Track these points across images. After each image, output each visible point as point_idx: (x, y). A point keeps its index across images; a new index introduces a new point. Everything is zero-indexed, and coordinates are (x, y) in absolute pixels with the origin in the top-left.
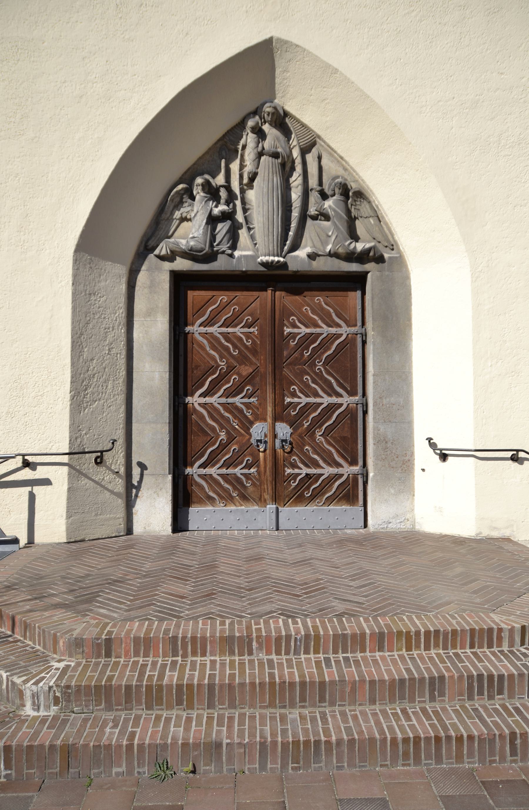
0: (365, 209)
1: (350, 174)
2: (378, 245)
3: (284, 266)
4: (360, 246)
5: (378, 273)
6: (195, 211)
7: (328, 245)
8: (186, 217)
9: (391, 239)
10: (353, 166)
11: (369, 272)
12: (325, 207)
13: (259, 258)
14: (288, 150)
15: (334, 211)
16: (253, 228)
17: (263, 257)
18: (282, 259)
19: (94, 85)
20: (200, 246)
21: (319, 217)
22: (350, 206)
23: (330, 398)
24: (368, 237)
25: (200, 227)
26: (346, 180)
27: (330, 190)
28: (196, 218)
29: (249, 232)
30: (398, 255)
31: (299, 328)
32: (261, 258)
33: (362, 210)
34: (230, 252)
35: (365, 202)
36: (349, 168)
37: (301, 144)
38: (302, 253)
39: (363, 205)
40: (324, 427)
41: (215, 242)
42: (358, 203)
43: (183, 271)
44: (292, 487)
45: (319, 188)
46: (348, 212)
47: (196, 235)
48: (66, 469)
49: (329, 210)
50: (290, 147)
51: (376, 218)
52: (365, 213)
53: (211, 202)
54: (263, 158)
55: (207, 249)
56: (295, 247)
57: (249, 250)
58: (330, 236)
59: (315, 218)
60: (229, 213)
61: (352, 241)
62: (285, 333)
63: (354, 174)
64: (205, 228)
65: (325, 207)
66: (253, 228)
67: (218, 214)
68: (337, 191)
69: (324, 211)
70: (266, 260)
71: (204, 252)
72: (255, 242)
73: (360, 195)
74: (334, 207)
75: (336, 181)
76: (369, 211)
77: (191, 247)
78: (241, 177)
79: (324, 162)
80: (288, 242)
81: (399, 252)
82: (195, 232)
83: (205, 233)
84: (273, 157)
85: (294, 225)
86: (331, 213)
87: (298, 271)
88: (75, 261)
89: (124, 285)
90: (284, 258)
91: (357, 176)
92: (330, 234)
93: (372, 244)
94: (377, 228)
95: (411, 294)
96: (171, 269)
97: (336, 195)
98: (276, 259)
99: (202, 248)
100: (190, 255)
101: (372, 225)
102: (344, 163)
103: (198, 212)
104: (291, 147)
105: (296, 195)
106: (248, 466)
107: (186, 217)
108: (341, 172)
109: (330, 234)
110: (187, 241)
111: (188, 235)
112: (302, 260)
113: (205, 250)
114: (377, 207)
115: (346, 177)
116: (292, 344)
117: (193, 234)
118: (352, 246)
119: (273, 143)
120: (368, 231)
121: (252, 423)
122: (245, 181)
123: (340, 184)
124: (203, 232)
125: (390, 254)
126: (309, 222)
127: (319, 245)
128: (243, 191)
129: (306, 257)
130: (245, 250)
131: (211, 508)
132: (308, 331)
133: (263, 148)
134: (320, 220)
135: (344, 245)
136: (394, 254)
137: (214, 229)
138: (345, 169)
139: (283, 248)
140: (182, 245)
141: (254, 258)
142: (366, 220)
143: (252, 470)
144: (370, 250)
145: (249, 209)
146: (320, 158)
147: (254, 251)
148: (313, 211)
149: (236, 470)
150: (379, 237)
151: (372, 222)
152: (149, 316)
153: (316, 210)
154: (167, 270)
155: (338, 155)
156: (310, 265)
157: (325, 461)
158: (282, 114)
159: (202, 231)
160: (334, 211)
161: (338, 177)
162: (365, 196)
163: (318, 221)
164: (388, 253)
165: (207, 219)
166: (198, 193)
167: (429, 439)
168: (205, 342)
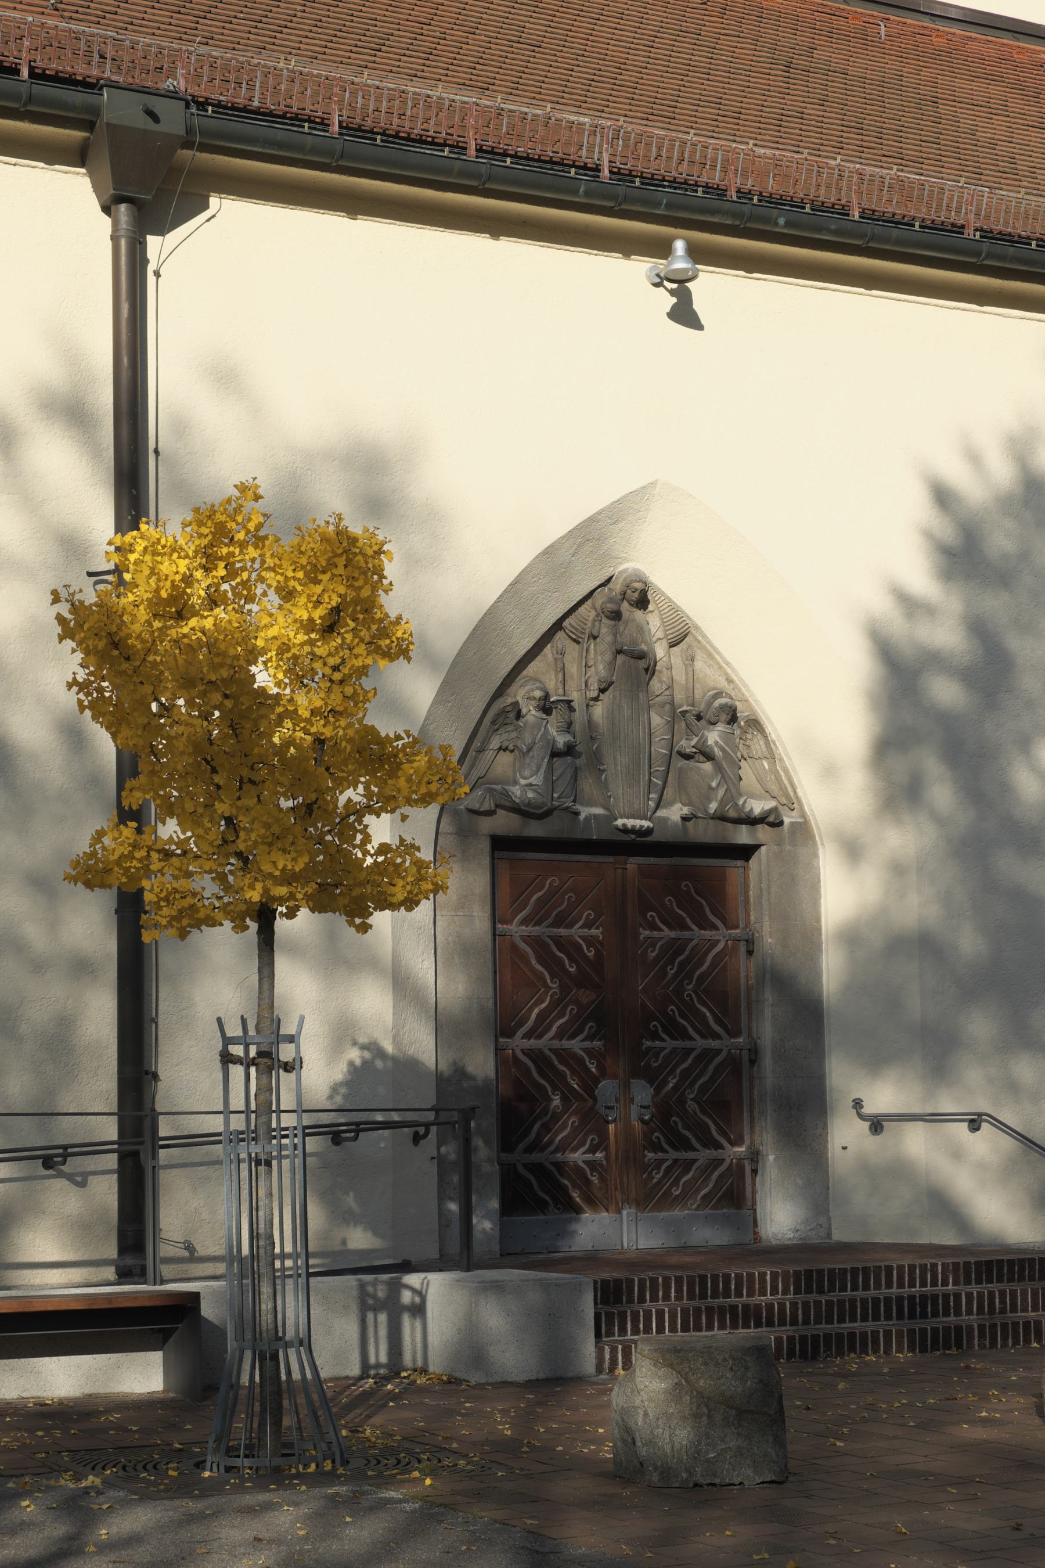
0: (757, 747)
1: (736, 687)
2: (780, 806)
3: (649, 831)
7: (710, 801)
16: (604, 771)
18: (646, 824)
23: (704, 1041)
28: (531, 754)
30: (801, 820)
31: (660, 930)
33: (753, 747)
35: (759, 736)
36: (735, 678)
39: (755, 740)
40: (696, 1087)
42: (749, 736)
44: (655, 1180)
48: (116, 1155)
59: (688, 757)
62: (642, 937)
66: (604, 771)
69: (707, 750)
71: (545, 809)
73: (755, 724)
76: (764, 749)
81: (803, 815)
86: (718, 752)
91: (746, 693)
92: (714, 784)
95: (819, 881)
98: (638, 823)
102: (729, 671)
106: (593, 1150)
108: (722, 683)
109: (714, 784)
116: (652, 955)
121: (597, 1081)
129: (679, 819)
131: (542, 1217)
132: (673, 934)
135: (736, 804)
138: (730, 681)
143: (599, 1155)
149: (576, 1155)
151: (767, 767)
152: (462, 907)
156: (685, 828)
157: (699, 1140)
160: (722, 749)
161: (719, 695)
163: (691, 763)
164: (791, 817)
167: (219, 1020)
168: (528, 950)
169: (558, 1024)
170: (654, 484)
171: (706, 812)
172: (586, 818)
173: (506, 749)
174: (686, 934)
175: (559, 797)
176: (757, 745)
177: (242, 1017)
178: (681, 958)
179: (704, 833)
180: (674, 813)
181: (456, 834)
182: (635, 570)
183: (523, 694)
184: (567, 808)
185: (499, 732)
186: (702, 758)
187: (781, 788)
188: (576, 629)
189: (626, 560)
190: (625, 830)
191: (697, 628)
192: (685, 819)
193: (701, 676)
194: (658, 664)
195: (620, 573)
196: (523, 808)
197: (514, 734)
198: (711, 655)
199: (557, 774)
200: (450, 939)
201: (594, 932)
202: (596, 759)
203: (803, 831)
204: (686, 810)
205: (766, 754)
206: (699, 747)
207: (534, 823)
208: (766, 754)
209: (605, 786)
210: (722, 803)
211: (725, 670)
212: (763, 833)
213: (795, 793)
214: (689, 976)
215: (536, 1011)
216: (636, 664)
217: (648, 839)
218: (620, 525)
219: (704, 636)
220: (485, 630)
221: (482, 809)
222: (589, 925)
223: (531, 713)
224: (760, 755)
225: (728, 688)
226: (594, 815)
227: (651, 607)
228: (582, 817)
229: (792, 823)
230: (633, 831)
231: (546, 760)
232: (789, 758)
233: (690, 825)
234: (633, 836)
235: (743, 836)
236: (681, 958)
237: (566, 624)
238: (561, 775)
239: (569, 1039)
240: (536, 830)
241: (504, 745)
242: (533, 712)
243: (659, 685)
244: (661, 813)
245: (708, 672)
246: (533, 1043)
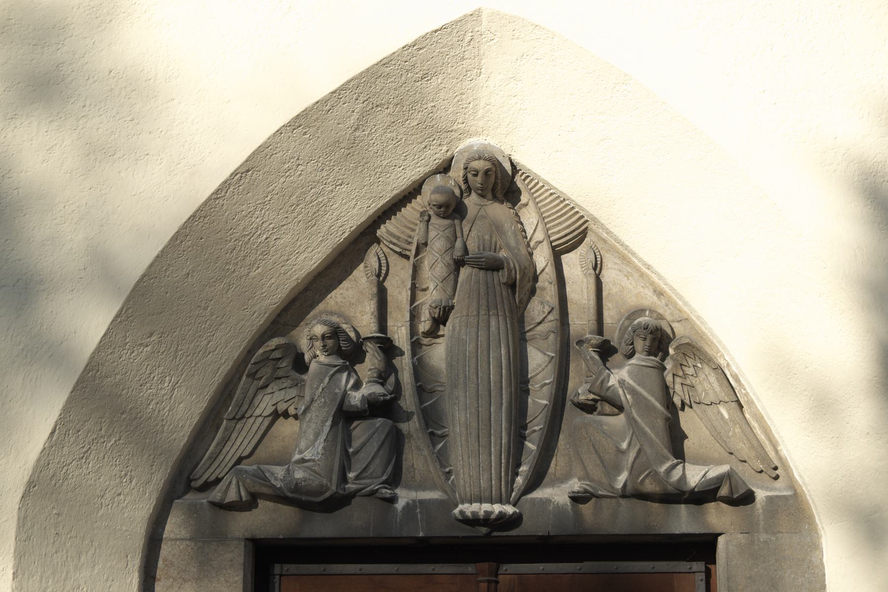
0: (706, 384)
1: (670, 302)
2: (740, 469)
3: (515, 521)
4: (695, 476)
5: (740, 536)
6: (307, 398)
7: (619, 472)
8: (286, 410)
9: (772, 454)
10: (675, 287)
11: (720, 534)
12: (610, 384)
13: (457, 506)
14: (523, 251)
15: (633, 392)
16: (443, 436)
17: (466, 505)
18: (509, 509)
19: (81, 122)
20: (315, 482)
21: (599, 405)
22: (669, 379)
24: (717, 450)
25: (317, 435)
26: (661, 317)
27: (623, 344)
28: (308, 416)
29: (434, 445)
30: (788, 493)
32: (460, 507)
33: (699, 388)
34: (386, 492)
35: (707, 369)
36: (666, 288)
37: (554, 244)
38: (556, 494)
39: (702, 376)
41: (350, 446)
42: (690, 371)
43: (278, 539)
45: (596, 339)
46: (666, 392)
47: (307, 455)
49: (621, 392)
50: (528, 245)
51: (734, 405)
52: (707, 394)
53: (345, 375)
54: (464, 272)
55: (334, 488)
56: (536, 480)
57: (433, 487)
58: (623, 452)
59: (588, 408)
60: (385, 401)
61: (675, 461)
63: (680, 303)
64: (330, 438)
65: (610, 384)
66: (443, 436)
67: (359, 404)
68: (640, 345)
69: (609, 394)
70: (472, 513)
71: (327, 495)
72: (447, 470)
73: (696, 351)
74: (631, 382)
75: (636, 322)
77: (297, 484)
78: (414, 316)
79: (609, 276)
80: (524, 469)
81: (792, 485)
82: (307, 448)
83: (328, 450)
84: (487, 269)
85: (536, 426)
86: (626, 398)
87: (549, 537)
88: (22, 522)
89: (136, 575)
90: (514, 505)
91: (685, 309)
92: (624, 445)
93: (724, 469)
94: (737, 430)
96: (248, 536)
97: (637, 355)
98: (497, 508)
99: (322, 486)
100: (296, 498)
101: (725, 422)
102: (655, 279)
103: (312, 401)
104: (532, 244)
105: (539, 360)
107: (286, 410)
108: (648, 298)
110: (288, 470)
111: (291, 457)
112: (560, 510)
113: (328, 489)
114: (737, 380)
115: (661, 311)
117: (301, 452)
118: (677, 474)
119: (487, 237)
120: (717, 436)
122: (424, 326)
123: (646, 328)
124: (324, 448)
125: (771, 490)
126: (572, 418)
127: (597, 472)
128: (416, 346)
129: (568, 501)
130: (424, 489)
133: (466, 251)
134: (600, 414)
135: (656, 473)
136: (780, 489)
137: (348, 440)
138: (659, 293)
139: (513, 481)
140: (276, 479)
141: (448, 505)
142: (710, 410)
144: (720, 480)
145: (432, 392)
146: (597, 267)
147: (445, 492)
148: (584, 394)
150: (743, 448)
151: (726, 415)
153: (590, 392)
154: (238, 539)
155: (640, 260)
156: (578, 515)
158: (510, 173)
159: (322, 445)
161: (641, 311)
162: (705, 354)
163: (594, 417)
164: (767, 489)
165: (334, 416)
166: (315, 356)
170: (475, 16)
171: (613, 488)
172: (408, 508)
173: (286, 415)
175: (357, 478)
176: (707, 384)
179: (623, 519)
180: (556, 494)
181: (191, 539)
182: (485, 146)
183: (309, 335)
184: (372, 493)
185: (269, 390)
186: (608, 408)
187: (752, 447)
188: (398, 238)
189: (466, 134)
190: (473, 521)
191: (595, 220)
192: (577, 499)
193: (614, 290)
194: (541, 278)
195: (460, 152)
196: (289, 494)
197: (293, 392)
198: (625, 258)
199: (356, 444)
202: (433, 421)
203: (793, 509)
204: (576, 485)
205: (723, 396)
206: (596, 390)
207: (319, 517)
208: (723, 396)
209: (442, 458)
210: (634, 471)
211: (647, 276)
212: (717, 517)
213: (777, 452)
216: (507, 284)
217: (513, 533)
218: (435, 82)
219: (609, 232)
220: (207, 234)
221: (227, 500)
223: (319, 359)
224: (712, 398)
225: (660, 305)
226: (422, 502)
227: (524, 198)
228: (400, 505)
229: (770, 500)
230: (486, 521)
231: (329, 423)
232: (759, 400)
233: (587, 509)
234: (484, 530)
235: (682, 521)
237: (381, 232)
238: (363, 445)
240: (324, 527)
241: (281, 407)
242: (322, 358)
243: (540, 307)
244: (538, 494)
245: (627, 283)
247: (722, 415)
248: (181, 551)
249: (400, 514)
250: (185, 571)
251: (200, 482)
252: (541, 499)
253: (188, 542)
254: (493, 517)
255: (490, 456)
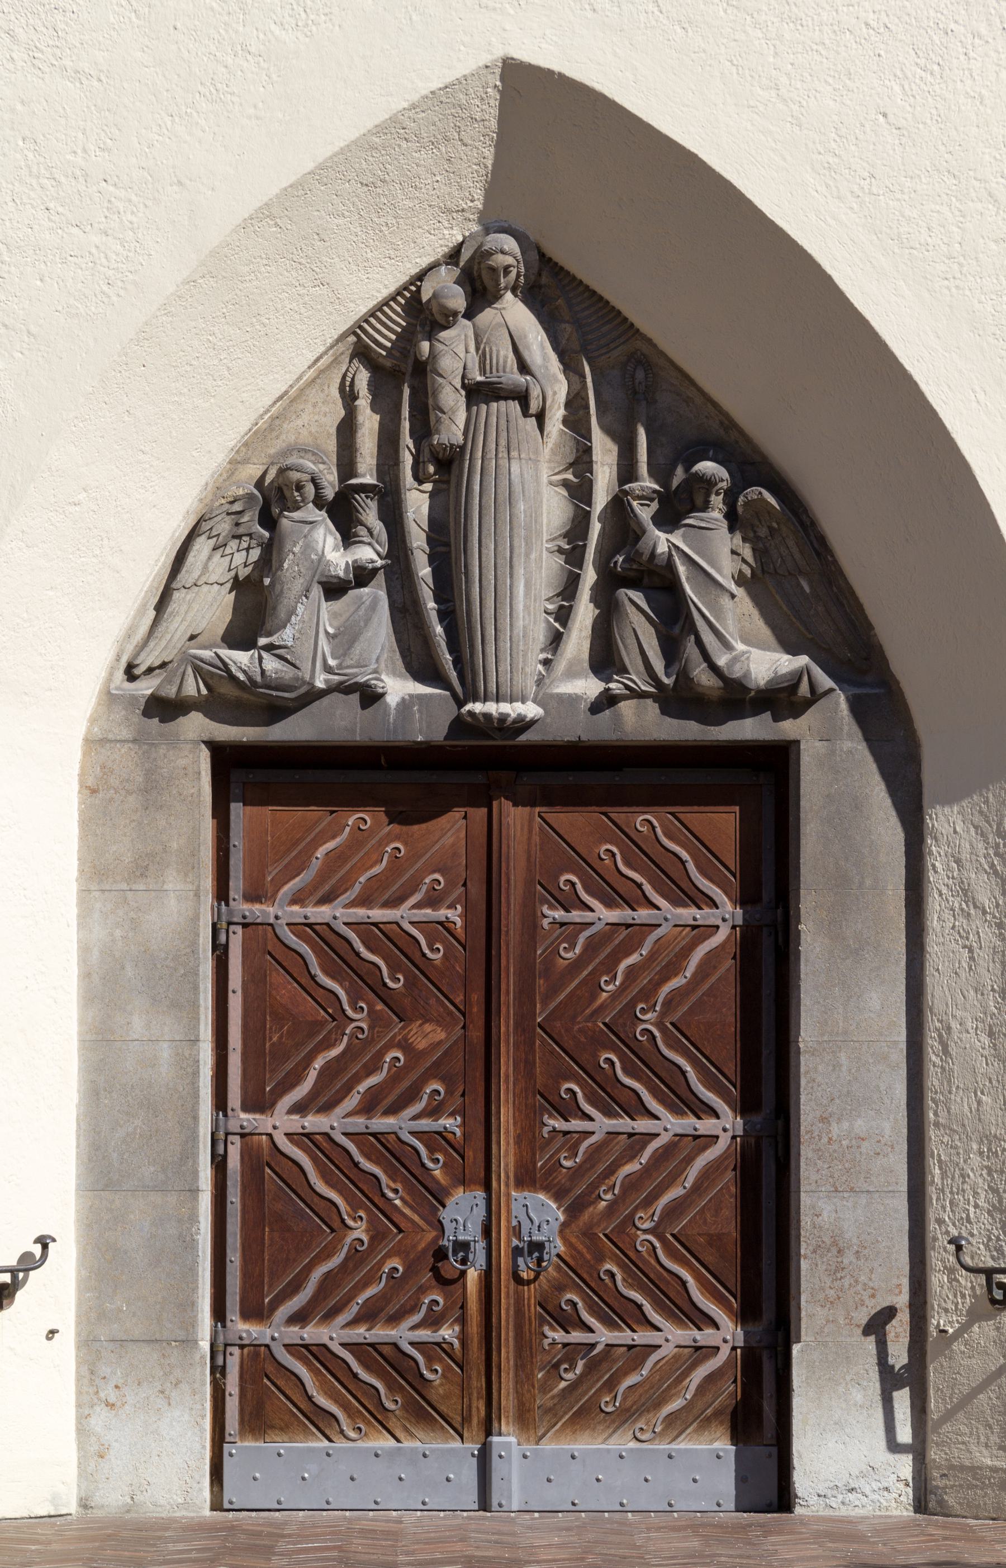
5: (818, 744)
151: (807, 589)
157: (660, 1307)
169: (362, 1088)
174: (643, 915)
177: (718, 1329)
178: (633, 959)
181: (134, 741)
200: (118, 933)
201: (443, 913)
214: (648, 994)
215: (318, 1064)
217: (523, 738)
222: (432, 901)
236: (633, 959)
239: (387, 1113)
246: (313, 1122)
247: (802, 587)
248: (122, 757)
249: (393, 712)
250: (128, 781)
251: (143, 668)
252: (570, 695)
253: (130, 745)
254: (510, 720)
255: (776, 1147)
